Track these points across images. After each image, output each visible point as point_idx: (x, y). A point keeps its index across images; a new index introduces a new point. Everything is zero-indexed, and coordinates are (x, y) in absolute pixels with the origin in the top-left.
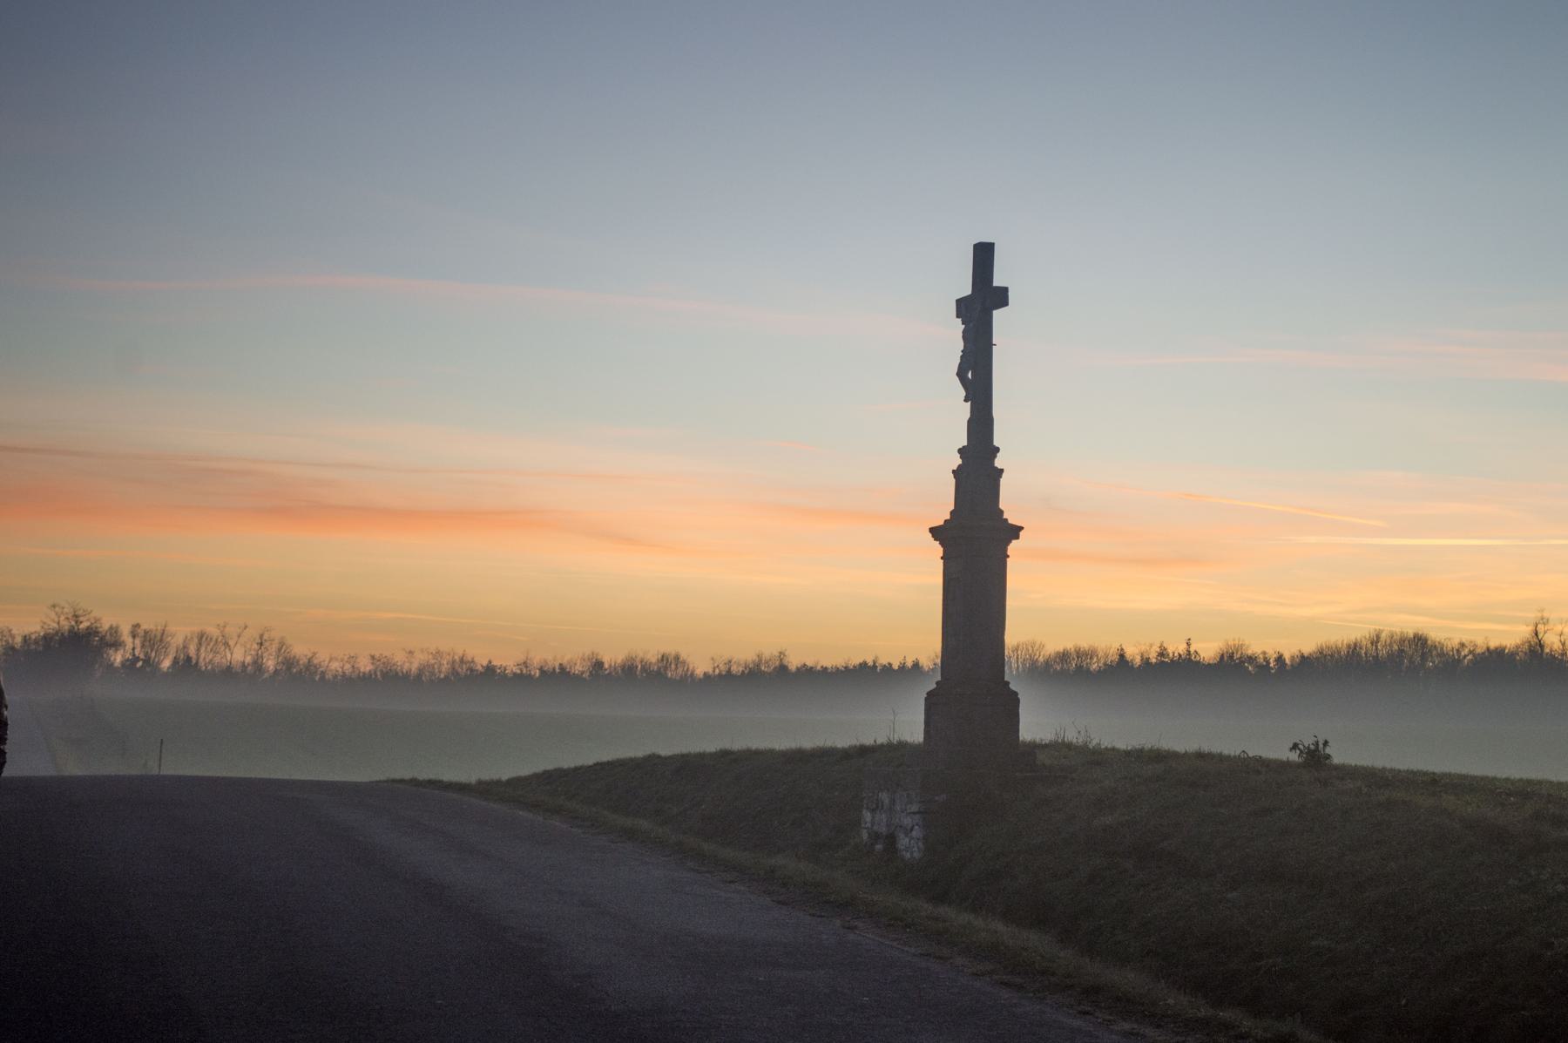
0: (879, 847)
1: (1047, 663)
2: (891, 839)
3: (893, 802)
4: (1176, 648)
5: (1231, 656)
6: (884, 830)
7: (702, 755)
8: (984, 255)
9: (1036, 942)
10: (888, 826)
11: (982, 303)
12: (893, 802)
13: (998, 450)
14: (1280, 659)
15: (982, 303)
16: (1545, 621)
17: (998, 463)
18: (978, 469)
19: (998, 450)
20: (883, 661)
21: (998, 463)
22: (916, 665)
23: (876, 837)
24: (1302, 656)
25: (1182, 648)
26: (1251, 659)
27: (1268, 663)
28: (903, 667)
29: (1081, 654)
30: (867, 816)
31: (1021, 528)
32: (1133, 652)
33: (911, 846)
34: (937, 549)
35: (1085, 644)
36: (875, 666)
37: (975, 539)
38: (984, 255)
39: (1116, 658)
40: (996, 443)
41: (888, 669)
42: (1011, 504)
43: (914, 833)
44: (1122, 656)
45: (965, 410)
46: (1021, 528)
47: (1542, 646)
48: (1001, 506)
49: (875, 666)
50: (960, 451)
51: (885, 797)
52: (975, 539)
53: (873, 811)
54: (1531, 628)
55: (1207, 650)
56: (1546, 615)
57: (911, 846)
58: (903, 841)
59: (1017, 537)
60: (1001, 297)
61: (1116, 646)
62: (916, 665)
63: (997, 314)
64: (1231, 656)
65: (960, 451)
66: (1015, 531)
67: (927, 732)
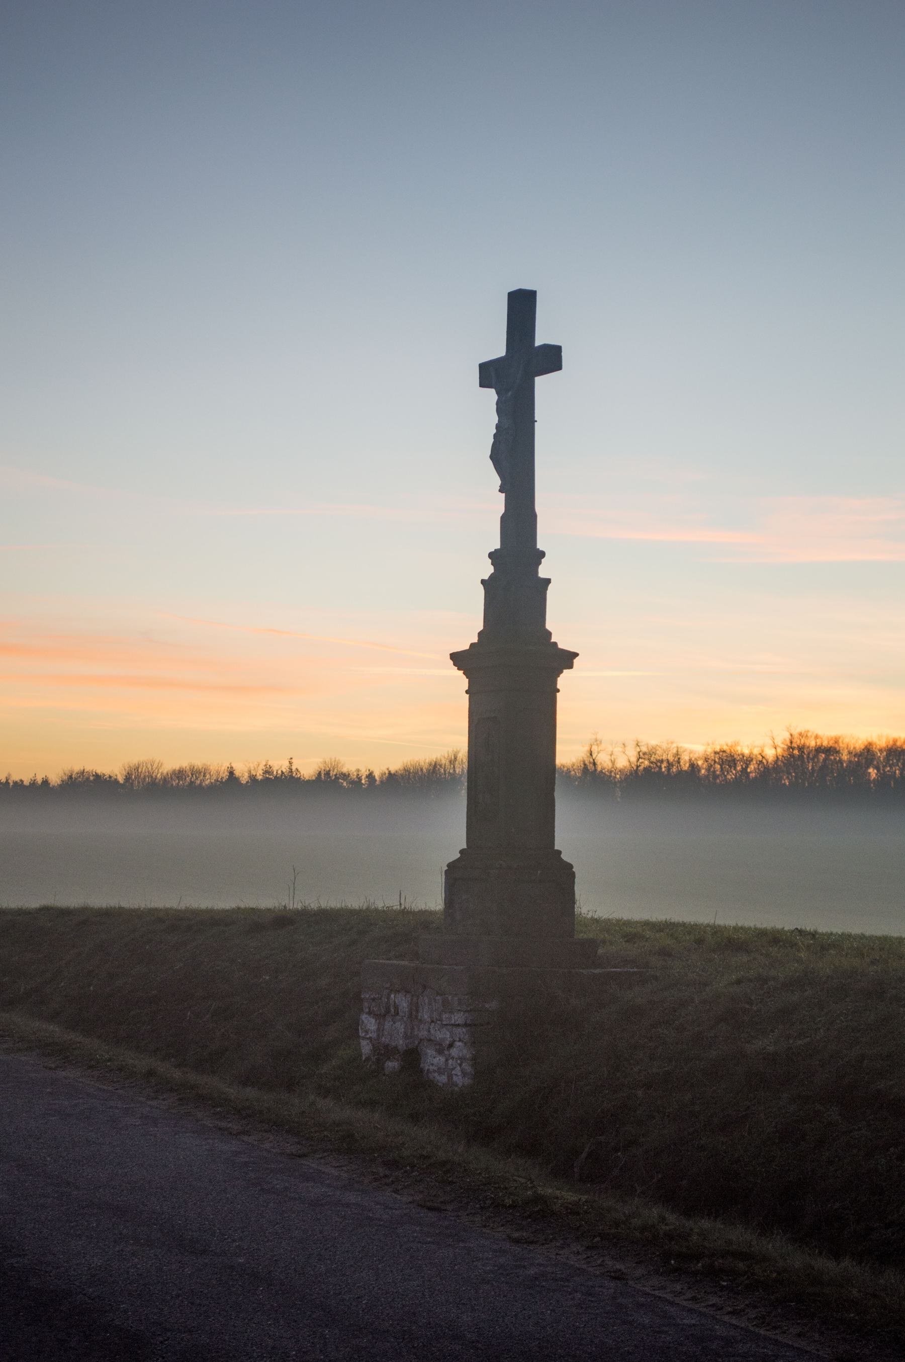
0: (392, 1065)
1: (165, 780)
2: (412, 1057)
3: (414, 1009)
4: (280, 765)
5: (328, 773)
6: (401, 1043)
7: (21, 912)
8: (522, 305)
9: (781, 1252)
10: (406, 1037)
11: (519, 369)
12: (414, 1009)
13: (542, 554)
14: (370, 776)
15: (519, 369)
16: (598, 742)
17: (543, 572)
18: (516, 580)
19: (542, 554)
20: (16, 777)
21: (543, 572)
22: (45, 782)
23: (384, 1052)
24: (390, 773)
25: (285, 769)
26: (345, 776)
27: (360, 779)
28: (33, 784)
29: (196, 772)
30: (369, 1023)
31: (576, 655)
32: (242, 771)
33: (450, 1064)
34: (461, 681)
35: (198, 763)
36: (7, 782)
37: (514, 661)
38: (522, 305)
39: (225, 775)
40: (540, 546)
41: (19, 785)
42: (562, 624)
43: (454, 1052)
44: (231, 773)
45: (498, 504)
46: (576, 655)
47: (594, 764)
48: (549, 626)
49: (7, 782)
50: (491, 555)
51: (403, 1002)
52: (514, 661)
53: (380, 1017)
54: (587, 748)
55: (307, 769)
56: (599, 737)
57: (450, 1064)
58: (432, 1060)
59: (570, 666)
60: (489, 374)
61: (226, 765)
62: (45, 782)
63: (542, 383)
64: (328, 773)
65: (491, 555)
66: (567, 659)
67: (449, 901)
